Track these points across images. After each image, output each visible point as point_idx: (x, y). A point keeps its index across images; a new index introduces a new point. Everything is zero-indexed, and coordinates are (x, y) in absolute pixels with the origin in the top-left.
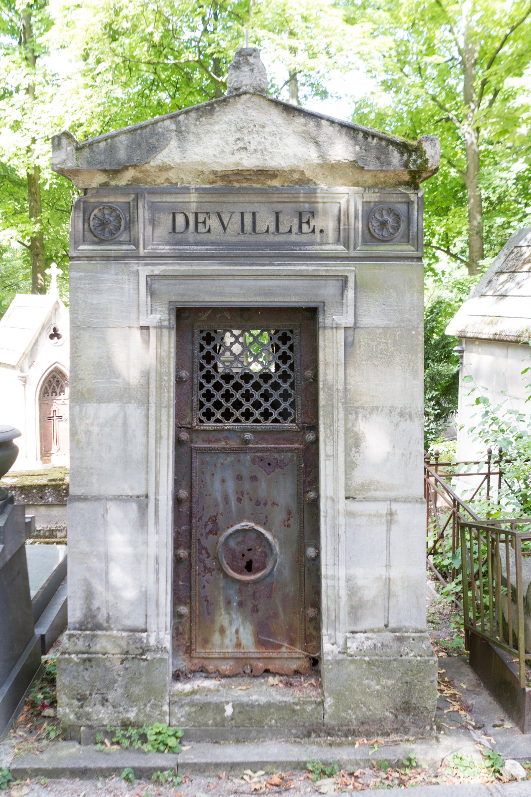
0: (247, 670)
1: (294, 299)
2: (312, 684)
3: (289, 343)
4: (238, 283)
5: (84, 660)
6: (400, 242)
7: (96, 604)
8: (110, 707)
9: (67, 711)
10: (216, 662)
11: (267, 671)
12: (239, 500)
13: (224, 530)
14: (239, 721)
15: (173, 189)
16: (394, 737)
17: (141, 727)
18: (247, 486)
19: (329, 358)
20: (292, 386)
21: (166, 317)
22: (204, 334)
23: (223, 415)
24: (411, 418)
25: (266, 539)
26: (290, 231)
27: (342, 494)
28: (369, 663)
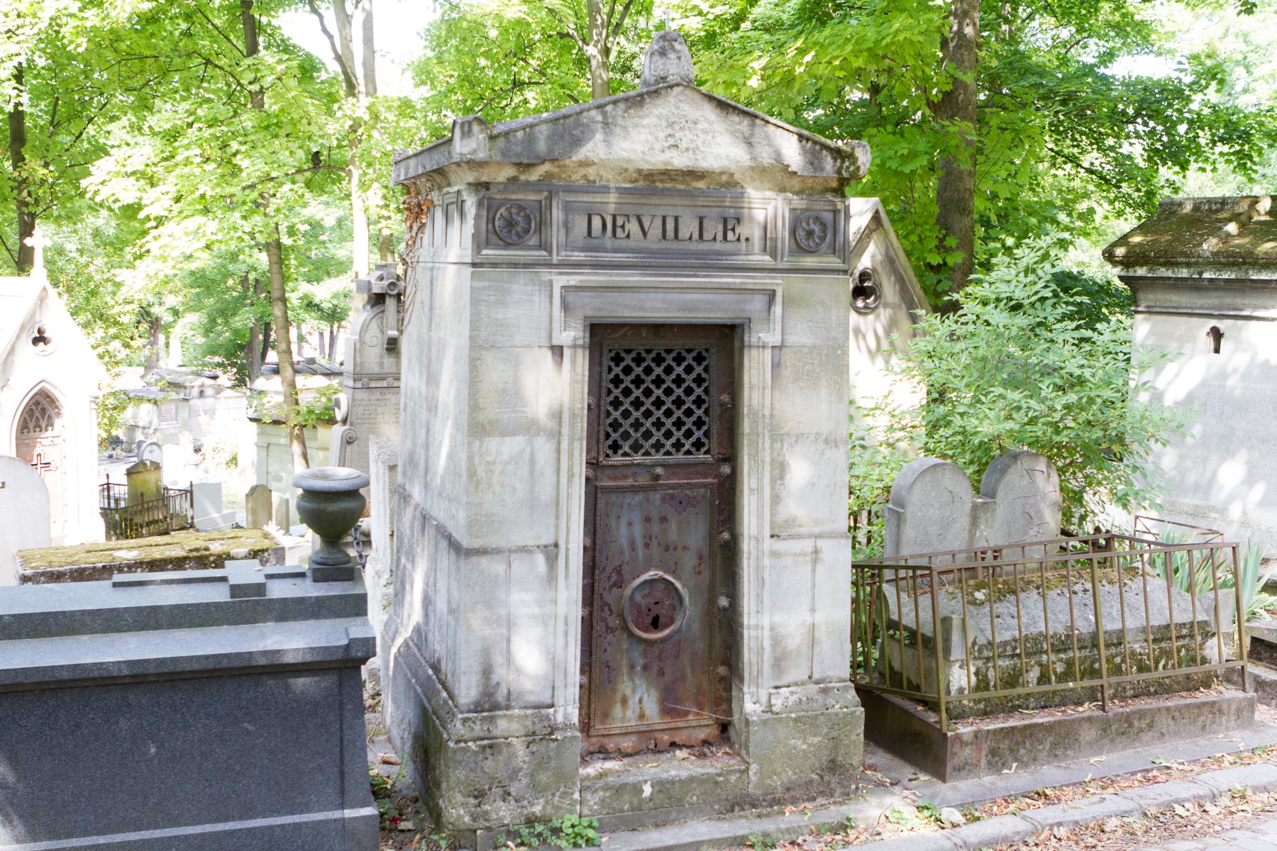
0: (653, 745)
1: (718, 315)
2: (727, 754)
3: (704, 364)
4: (661, 296)
5: (484, 747)
6: (825, 254)
7: (495, 678)
8: (513, 802)
9: (462, 812)
10: (617, 739)
11: (673, 745)
12: (647, 545)
13: (629, 582)
14: (657, 801)
15: (591, 187)
16: (821, 800)
17: (551, 820)
18: (656, 528)
19: (755, 381)
20: (706, 412)
21: (581, 334)
22: (613, 354)
23: (631, 447)
24: (836, 446)
25: (676, 589)
26: (715, 239)
27: (767, 533)
28: (796, 720)
